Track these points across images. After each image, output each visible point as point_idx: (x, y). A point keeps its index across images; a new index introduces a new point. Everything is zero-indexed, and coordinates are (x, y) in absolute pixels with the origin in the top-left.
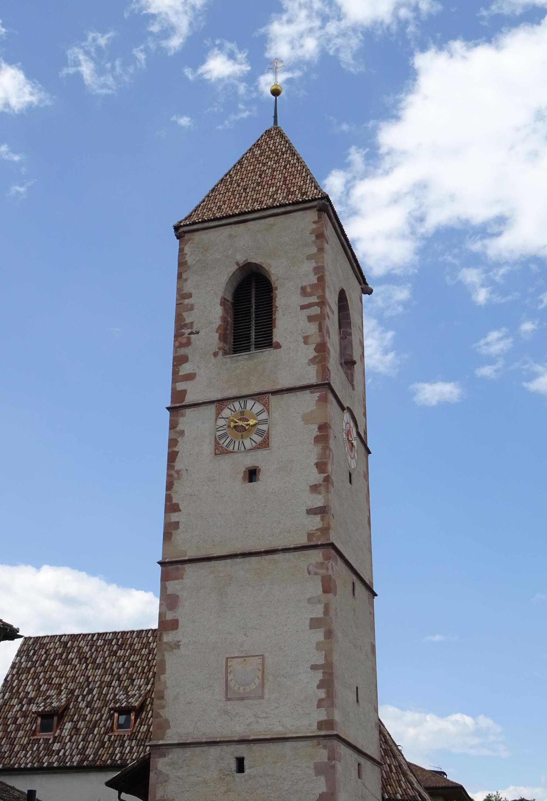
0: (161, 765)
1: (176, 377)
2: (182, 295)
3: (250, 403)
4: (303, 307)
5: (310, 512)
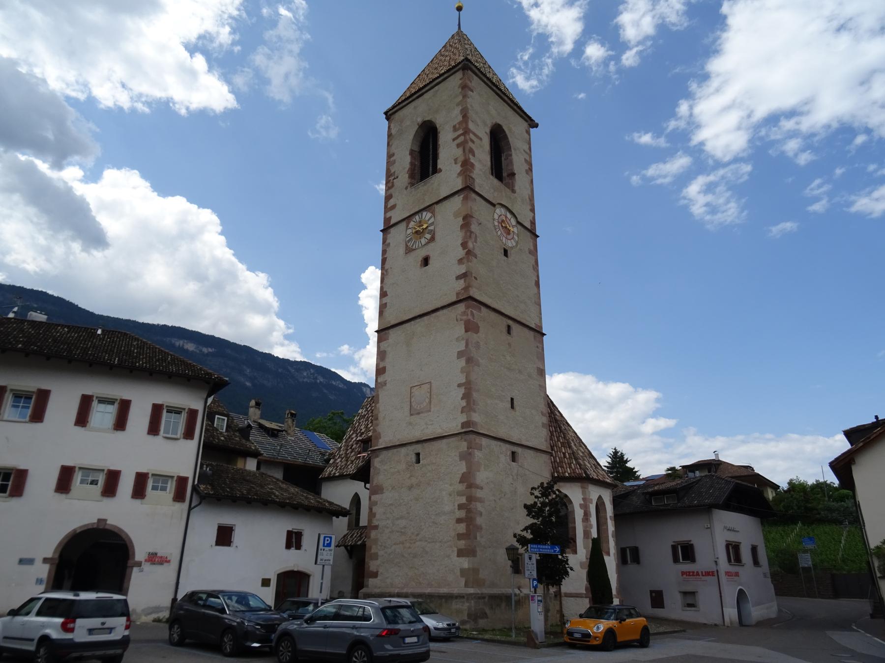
0: (376, 463)
1: (387, 209)
2: (390, 156)
3: (424, 213)
4: (454, 140)
5: (459, 278)
